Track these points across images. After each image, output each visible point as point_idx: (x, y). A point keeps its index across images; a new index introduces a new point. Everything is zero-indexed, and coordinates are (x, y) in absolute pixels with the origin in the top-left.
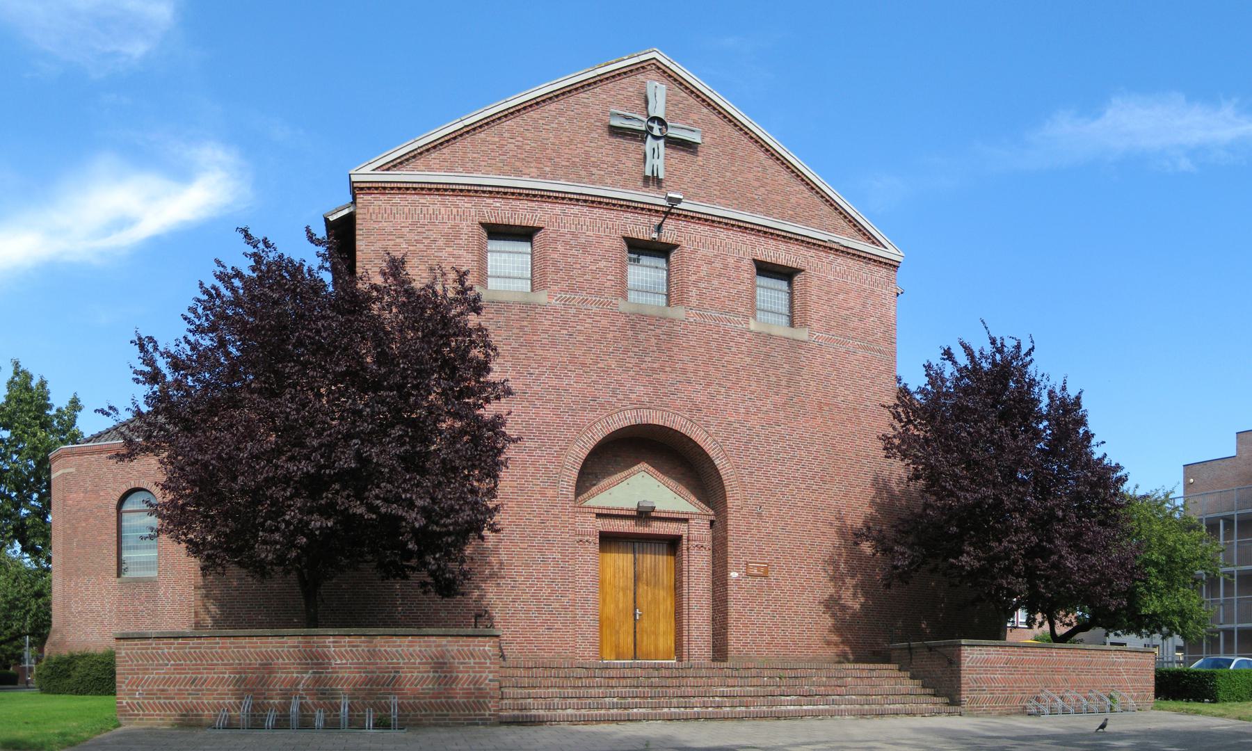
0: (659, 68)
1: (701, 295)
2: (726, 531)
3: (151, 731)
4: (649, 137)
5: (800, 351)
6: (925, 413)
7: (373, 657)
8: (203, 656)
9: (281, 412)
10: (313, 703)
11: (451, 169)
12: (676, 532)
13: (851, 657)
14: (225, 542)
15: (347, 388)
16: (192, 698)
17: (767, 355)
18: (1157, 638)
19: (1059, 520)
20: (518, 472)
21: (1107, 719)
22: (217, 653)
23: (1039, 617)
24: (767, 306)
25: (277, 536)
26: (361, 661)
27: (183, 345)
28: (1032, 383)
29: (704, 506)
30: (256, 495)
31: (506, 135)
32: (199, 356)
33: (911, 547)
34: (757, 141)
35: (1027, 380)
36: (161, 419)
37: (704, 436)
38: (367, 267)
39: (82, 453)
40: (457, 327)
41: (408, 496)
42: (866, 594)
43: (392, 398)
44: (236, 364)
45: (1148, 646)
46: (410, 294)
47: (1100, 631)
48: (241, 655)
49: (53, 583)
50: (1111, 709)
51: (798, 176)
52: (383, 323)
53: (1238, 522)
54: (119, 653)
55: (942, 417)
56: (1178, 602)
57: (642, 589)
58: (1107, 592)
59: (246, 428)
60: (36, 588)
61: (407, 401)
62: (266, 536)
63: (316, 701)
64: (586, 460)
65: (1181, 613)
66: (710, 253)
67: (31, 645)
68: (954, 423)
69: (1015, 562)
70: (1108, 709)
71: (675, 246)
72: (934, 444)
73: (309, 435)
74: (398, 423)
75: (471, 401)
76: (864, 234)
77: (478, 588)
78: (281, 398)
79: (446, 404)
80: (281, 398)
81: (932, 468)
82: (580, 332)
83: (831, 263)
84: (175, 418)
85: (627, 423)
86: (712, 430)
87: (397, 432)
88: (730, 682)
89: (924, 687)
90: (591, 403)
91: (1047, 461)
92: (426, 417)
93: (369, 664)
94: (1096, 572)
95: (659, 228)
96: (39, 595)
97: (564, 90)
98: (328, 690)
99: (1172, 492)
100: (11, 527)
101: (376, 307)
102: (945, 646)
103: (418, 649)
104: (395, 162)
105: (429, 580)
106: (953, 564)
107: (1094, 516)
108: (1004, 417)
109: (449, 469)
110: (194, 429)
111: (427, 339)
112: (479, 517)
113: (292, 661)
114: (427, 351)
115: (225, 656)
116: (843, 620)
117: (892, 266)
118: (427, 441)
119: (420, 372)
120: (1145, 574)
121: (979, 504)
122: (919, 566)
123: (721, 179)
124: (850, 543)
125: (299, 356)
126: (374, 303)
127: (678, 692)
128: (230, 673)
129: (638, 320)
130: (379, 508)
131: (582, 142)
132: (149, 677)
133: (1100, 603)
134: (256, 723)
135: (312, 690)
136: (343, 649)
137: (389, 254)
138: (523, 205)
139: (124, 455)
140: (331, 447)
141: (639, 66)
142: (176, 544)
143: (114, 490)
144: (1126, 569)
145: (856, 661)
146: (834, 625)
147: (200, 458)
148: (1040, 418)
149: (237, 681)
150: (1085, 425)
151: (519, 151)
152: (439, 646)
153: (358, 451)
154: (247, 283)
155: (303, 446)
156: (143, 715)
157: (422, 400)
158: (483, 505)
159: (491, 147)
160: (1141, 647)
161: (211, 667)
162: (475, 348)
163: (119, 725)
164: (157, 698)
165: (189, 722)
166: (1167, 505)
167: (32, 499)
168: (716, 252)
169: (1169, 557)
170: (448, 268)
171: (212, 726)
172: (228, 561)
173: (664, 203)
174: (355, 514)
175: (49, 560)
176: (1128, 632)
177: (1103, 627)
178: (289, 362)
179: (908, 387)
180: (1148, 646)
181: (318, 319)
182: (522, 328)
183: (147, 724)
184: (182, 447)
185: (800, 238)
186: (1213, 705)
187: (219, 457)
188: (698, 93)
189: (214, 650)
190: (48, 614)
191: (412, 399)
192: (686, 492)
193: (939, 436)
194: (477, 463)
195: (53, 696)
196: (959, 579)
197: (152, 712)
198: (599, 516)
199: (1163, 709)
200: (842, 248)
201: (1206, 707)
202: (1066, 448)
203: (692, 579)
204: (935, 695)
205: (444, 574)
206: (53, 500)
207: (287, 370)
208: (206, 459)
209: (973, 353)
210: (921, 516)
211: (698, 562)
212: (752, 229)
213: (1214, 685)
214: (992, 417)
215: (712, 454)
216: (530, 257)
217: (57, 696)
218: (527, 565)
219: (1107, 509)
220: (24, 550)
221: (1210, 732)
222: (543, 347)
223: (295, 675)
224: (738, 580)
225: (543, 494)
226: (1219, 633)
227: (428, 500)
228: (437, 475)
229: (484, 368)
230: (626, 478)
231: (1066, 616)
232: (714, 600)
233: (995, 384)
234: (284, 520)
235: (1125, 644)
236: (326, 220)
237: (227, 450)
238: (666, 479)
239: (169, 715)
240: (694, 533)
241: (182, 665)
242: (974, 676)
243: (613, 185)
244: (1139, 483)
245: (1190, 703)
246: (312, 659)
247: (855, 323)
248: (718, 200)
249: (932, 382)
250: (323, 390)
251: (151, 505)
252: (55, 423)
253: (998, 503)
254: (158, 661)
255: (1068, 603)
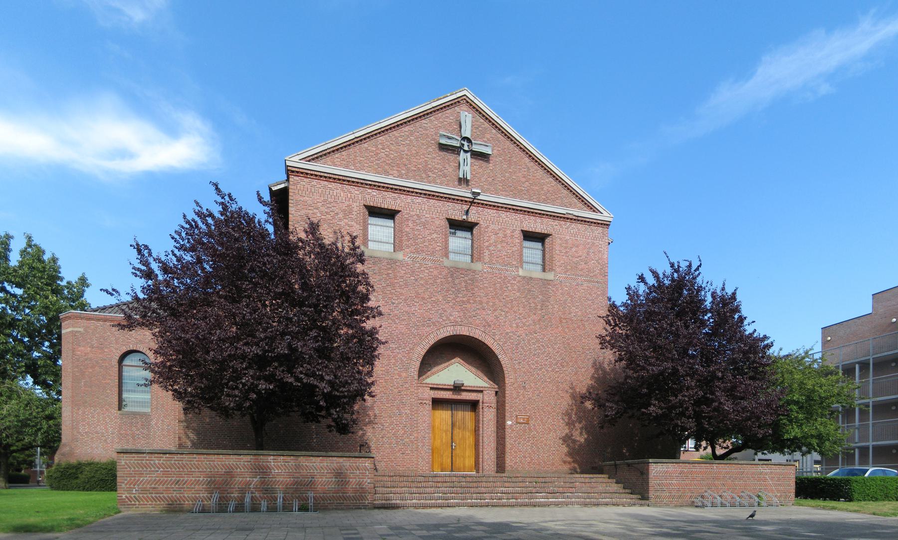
0: (468, 102)
1: (491, 255)
2: (504, 397)
3: (144, 516)
4: (462, 151)
5: (549, 287)
6: (626, 319)
7: (298, 468)
8: (185, 466)
9: (240, 313)
10: (260, 496)
11: (347, 167)
12: (476, 398)
13: (578, 470)
14: (201, 393)
15: (283, 303)
16: (176, 493)
17: (529, 291)
18: (797, 455)
19: (719, 379)
20: (385, 362)
21: (755, 511)
22: (194, 464)
23: (704, 444)
24: (529, 259)
25: (236, 392)
26: (291, 471)
27: (171, 256)
28: (700, 289)
29: (491, 383)
30: (222, 365)
31: (380, 146)
32: (183, 267)
33: (617, 403)
34: (524, 150)
35: (696, 288)
36: (154, 305)
37: (492, 341)
38: (296, 226)
39: (89, 319)
40: (350, 271)
41: (320, 373)
42: (588, 433)
43: (311, 312)
44: (208, 277)
45: (790, 461)
46: (322, 247)
47: (751, 452)
48: (211, 466)
49: (63, 410)
50: (759, 504)
51: (548, 172)
52: (305, 264)
53: (873, 364)
54: (119, 462)
55: (637, 320)
56: (816, 428)
57: (456, 431)
58: (756, 425)
59: (216, 320)
60: (47, 413)
61: (320, 315)
62: (229, 392)
63: (262, 495)
64: (424, 356)
65: (819, 437)
66: (496, 227)
67: (42, 454)
68: (645, 323)
69: (687, 409)
70: (756, 504)
71: (477, 224)
72: (632, 338)
73: (258, 330)
74: (314, 328)
75: (358, 318)
76: (588, 206)
77: (362, 429)
78: (240, 304)
79: (344, 319)
80: (240, 304)
81: (631, 353)
82: (422, 278)
83: (567, 228)
84: (164, 306)
85: (448, 334)
86: (497, 337)
87: (313, 333)
88: (507, 485)
89: (624, 488)
90: (428, 322)
91: (710, 340)
92: (332, 326)
93: (295, 473)
94: (747, 412)
95: (467, 212)
96: (50, 417)
97: (413, 117)
98: (269, 488)
99: (811, 350)
100: (23, 364)
101: (301, 253)
102: (638, 463)
103: (325, 464)
104: (313, 157)
105: (333, 424)
106: (643, 413)
107: (746, 373)
108: (680, 315)
109: (345, 358)
110: (179, 316)
111: (332, 277)
112: (363, 388)
113: (247, 470)
114: (332, 285)
115: (200, 467)
116: (574, 449)
117: (606, 225)
118: (332, 341)
119: (327, 297)
120: (787, 411)
121: (661, 373)
122: (622, 415)
123: (503, 178)
124: (578, 402)
125: (252, 278)
126: (300, 250)
127: (477, 490)
128: (204, 477)
129: (455, 271)
130: (302, 379)
131: (423, 154)
132: (144, 479)
133: (750, 432)
134: (222, 509)
135: (259, 488)
136: (279, 464)
137: (309, 219)
138: (389, 195)
139: (124, 326)
140: (272, 339)
141: (456, 101)
142: (165, 391)
143: (117, 349)
144: (771, 408)
145: (582, 473)
146: (568, 452)
147: (183, 336)
148: (705, 312)
149: (209, 482)
150: (739, 312)
151: (387, 158)
152: (339, 463)
153: (289, 343)
154: (217, 222)
155: (254, 336)
156: (139, 505)
157: (329, 315)
158: (365, 381)
159: (371, 154)
160: (784, 462)
161: (190, 474)
162: (361, 285)
163: (120, 512)
164: (150, 493)
165: (174, 508)
166: (807, 359)
167: (43, 345)
168: (500, 227)
169: (808, 397)
170: (345, 233)
171: (191, 511)
172: (202, 406)
173: (470, 195)
174: (287, 382)
175: (59, 393)
176: (773, 452)
177: (753, 449)
178: (245, 281)
179: (616, 303)
180: (790, 461)
181: (264, 256)
182: (388, 274)
183: (142, 510)
184: (170, 327)
185: (549, 213)
186: (848, 503)
187: (197, 337)
188: (490, 119)
189: (192, 463)
190: (58, 431)
191: (323, 314)
192: (481, 374)
193: (635, 332)
194: (361, 355)
195: (62, 492)
196: (647, 422)
197: (146, 503)
198: (432, 389)
199: (802, 505)
200: (574, 218)
201: (842, 504)
202: (724, 330)
203: (485, 425)
204: (631, 493)
205: (341, 420)
206: (63, 349)
207: (244, 286)
208: (187, 337)
209: (658, 275)
210: (623, 384)
211: (488, 415)
212: (521, 211)
213: (849, 489)
214: (671, 316)
215: (496, 352)
216: (393, 229)
217: (66, 492)
218: (391, 417)
219: (756, 368)
220: (35, 383)
221: (845, 523)
222: (400, 286)
223: (248, 479)
224: (511, 426)
225: (400, 376)
226: (854, 449)
227: (332, 376)
228: (338, 361)
229: (365, 298)
230: (447, 367)
231: (724, 442)
232: (497, 438)
233: (674, 294)
234: (241, 382)
235: (771, 460)
236: (270, 189)
237: (203, 333)
238: (470, 367)
239: (159, 505)
240: (486, 399)
241: (169, 471)
242: (658, 482)
243: (441, 184)
244: (782, 347)
245: (826, 502)
246: (259, 470)
247: (582, 265)
248: (501, 192)
249: (631, 299)
250: (267, 302)
251: (146, 363)
252: (66, 292)
253: (675, 371)
254: (151, 468)
255: (725, 433)
